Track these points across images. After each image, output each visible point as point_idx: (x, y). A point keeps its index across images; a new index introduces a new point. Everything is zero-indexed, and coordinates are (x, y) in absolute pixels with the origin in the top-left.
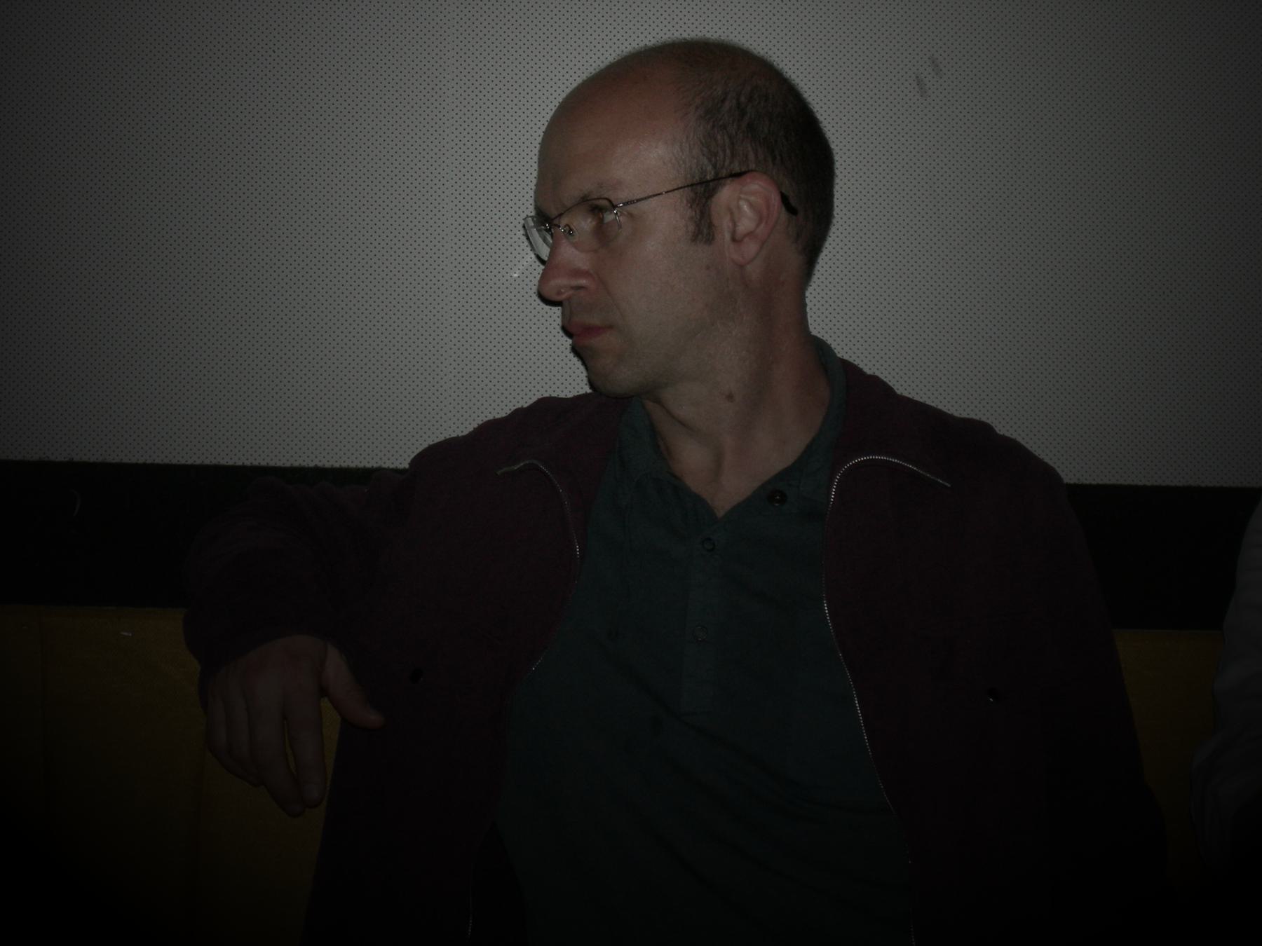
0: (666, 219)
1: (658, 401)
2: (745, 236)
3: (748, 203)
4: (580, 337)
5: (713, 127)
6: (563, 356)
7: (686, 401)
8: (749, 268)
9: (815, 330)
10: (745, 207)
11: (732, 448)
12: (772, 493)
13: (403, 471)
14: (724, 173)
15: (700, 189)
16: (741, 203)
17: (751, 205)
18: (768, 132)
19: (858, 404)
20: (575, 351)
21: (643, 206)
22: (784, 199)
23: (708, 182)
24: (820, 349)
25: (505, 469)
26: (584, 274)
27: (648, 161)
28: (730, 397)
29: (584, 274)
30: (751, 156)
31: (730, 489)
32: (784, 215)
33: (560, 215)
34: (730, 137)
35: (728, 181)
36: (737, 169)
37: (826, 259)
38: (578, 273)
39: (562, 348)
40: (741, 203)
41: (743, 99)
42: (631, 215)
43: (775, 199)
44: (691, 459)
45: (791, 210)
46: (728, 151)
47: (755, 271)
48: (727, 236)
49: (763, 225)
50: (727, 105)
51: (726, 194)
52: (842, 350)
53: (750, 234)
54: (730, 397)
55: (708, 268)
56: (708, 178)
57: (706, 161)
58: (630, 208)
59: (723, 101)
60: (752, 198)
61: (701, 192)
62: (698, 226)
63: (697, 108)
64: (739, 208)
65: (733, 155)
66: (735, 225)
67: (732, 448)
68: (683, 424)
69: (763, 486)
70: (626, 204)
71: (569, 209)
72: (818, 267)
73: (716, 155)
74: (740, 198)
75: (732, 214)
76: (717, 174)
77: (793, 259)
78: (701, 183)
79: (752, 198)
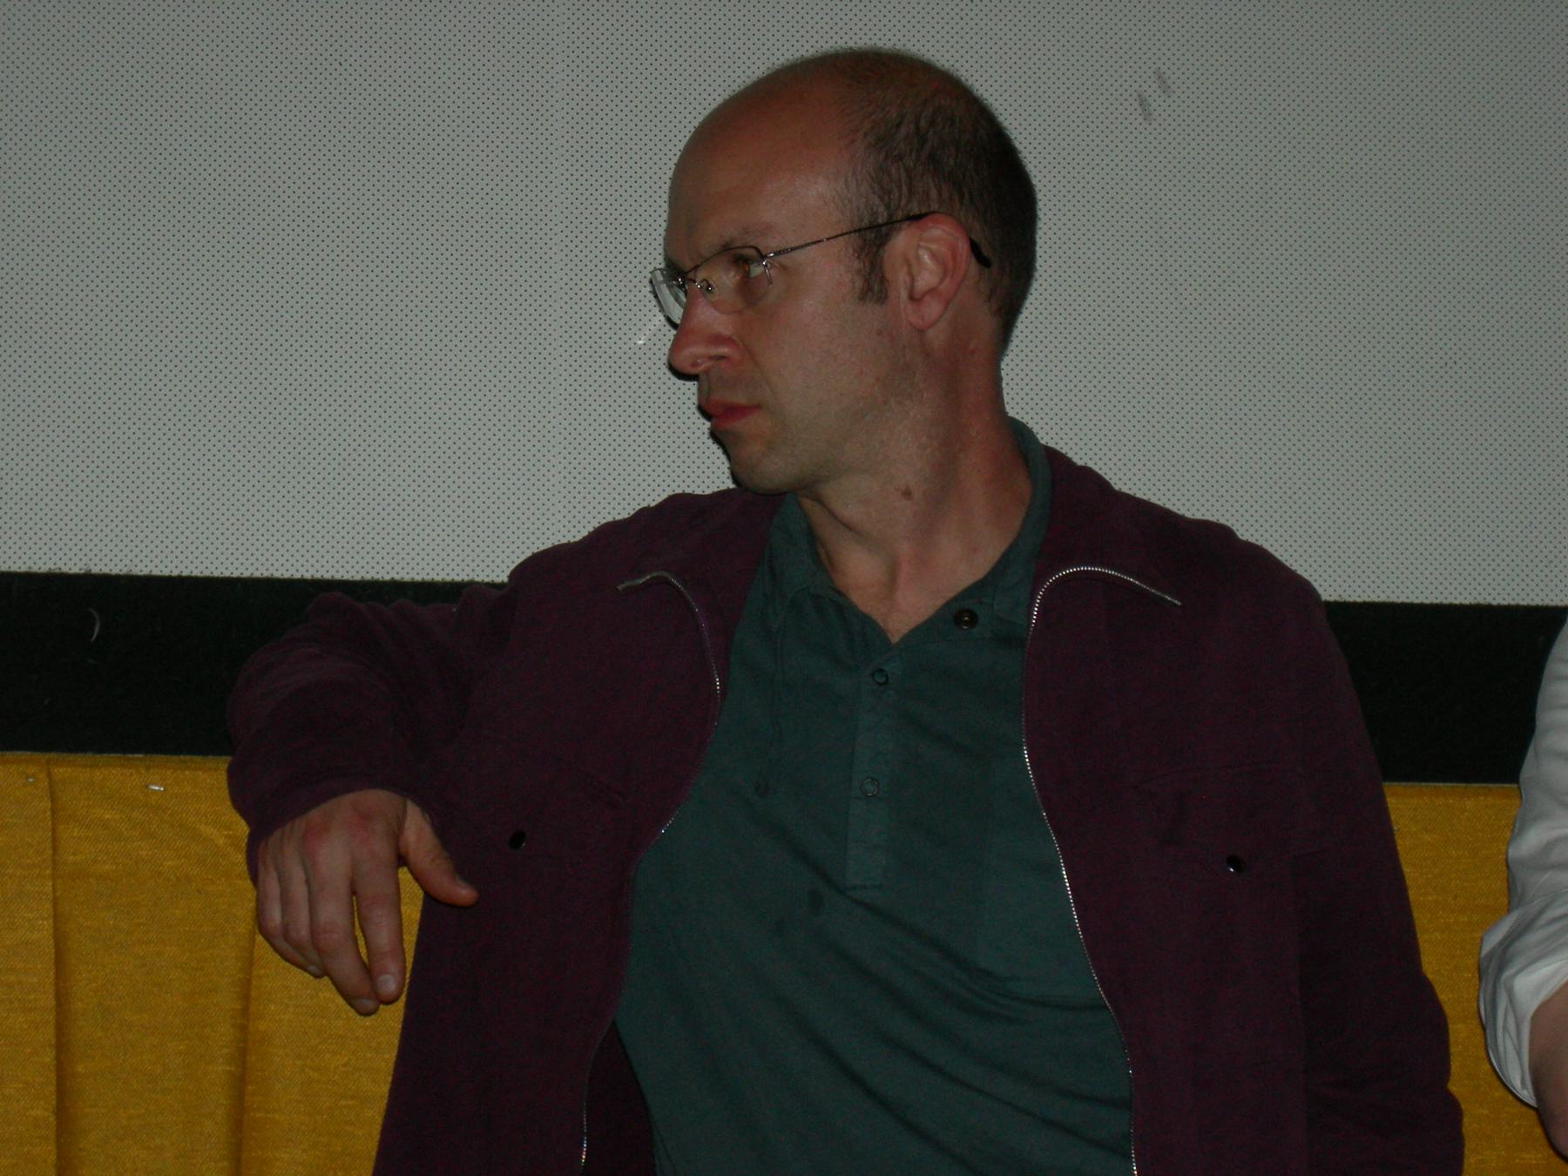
0: (827, 272)
1: (818, 499)
3: (929, 253)
4: (721, 419)
5: (886, 157)
7: (851, 498)
8: (931, 333)
10: (926, 258)
11: (910, 559)
12: (960, 613)
14: (900, 215)
16: (921, 252)
17: (933, 256)
18: (951, 168)
19: (1070, 506)
22: (975, 248)
25: (666, 574)
27: (806, 200)
30: (934, 194)
31: (906, 609)
32: (974, 267)
33: (696, 268)
34: (907, 170)
36: (915, 209)
38: (718, 340)
40: (921, 252)
41: (923, 123)
42: (784, 268)
43: (963, 248)
45: (983, 261)
46: (905, 189)
47: (937, 337)
48: (904, 294)
49: (947, 281)
50: (903, 131)
51: (902, 241)
53: (932, 291)
54: (907, 494)
55: (880, 333)
56: (880, 221)
57: (877, 201)
58: (783, 259)
59: (898, 126)
60: (934, 247)
61: (871, 239)
64: (918, 258)
65: (911, 192)
66: (913, 280)
67: (910, 559)
68: (848, 527)
69: (948, 603)
70: (778, 253)
72: (1016, 332)
73: (890, 193)
75: (909, 265)
76: (890, 216)
77: (985, 322)
78: (871, 228)
79: (934, 247)
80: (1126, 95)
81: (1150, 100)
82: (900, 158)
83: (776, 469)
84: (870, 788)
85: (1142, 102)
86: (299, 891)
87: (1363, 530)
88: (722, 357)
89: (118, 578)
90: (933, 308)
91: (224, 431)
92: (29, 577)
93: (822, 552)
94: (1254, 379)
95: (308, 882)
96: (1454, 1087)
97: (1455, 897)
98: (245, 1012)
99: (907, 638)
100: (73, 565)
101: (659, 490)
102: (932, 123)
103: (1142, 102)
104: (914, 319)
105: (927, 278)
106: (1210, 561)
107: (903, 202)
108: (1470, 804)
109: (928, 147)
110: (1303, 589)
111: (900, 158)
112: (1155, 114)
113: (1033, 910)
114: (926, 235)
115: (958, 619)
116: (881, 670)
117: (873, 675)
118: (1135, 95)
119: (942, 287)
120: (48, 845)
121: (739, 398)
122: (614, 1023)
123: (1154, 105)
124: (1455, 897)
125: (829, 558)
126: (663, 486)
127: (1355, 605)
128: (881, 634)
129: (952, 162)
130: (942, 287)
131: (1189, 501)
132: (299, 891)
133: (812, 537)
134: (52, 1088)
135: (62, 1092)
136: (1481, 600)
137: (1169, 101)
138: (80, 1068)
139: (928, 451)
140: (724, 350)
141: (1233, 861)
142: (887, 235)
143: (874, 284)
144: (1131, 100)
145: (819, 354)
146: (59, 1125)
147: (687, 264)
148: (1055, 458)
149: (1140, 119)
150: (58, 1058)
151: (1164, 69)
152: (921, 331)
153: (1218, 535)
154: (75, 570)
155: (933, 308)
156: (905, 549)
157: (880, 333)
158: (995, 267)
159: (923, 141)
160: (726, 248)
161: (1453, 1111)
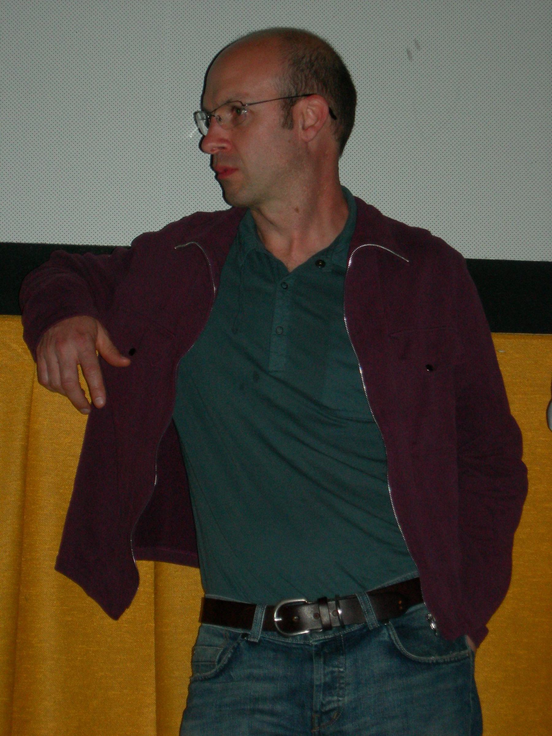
0: (269, 115)
1: (259, 211)
2: (309, 127)
3: (313, 110)
4: (221, 174)
5: (297, 70)
6: (210, 182)
7: (273, 210)
8: (310, 144)
9: (343, 182)
10: (311, 113)
11: (296, 237)
12: (318, 261)
13: (127, 247)
14: (301, 94)
15: (288, 101)
16: (309, 110)
17: (313, 112)
18: (323, 78)
19: (364, 220)
20: (216, 177)
21: (257, 107)
22: (331, 112)
23: (292, 97)
24: (345, 192)
25: (180, 246)
26: (226, 141)
27: (263, 86)
28: (297, 210)
29: (226, 141)
30: (315, 87)
31: (296, 259)
32: (329, 119)
33: (215, 110)
34: (305, 77)
35: (303, 98)
36: (308, 92)
37: (345, 160)
38: (222, 140)
39: (210, 178)
40: (309, 110)
41: (313, 58)
42: (251, 112)
43: (326, 110)
44: (277, 243)
45: (333, 117)
46: (304, 84)
47: (313, 146)
48: (300, 127)
49: (318, 123)
50: (304, 60)
51: (302, 105)
52: (355, 193)
53: (312, 127)
54: (297, 210)
55: (289, 141)
56: (293, 95)
57: (292, 87)
58: (251, 108)
59: (303, 58)
60: (314, 109)
61: (289, 102)
62: (286, 119)
63: (289, 60)
64: (307, 112)
65: (306, 85)
66: (304, 121)
67: (296, 237)
68: (271, 223)
69: (313, 257)
70: (250, 104)
71: (219, 107)
72: (346, 146)
73: (297, 84)
74: (308, 108)
75: (303, 115)
76: (297, 94)
77: (333, 144)
78: (288, 98)
79: (314, 109)
81: (412, 52)
82: (303, 70)
83: (244, 196)
84: (280, 331)
87: (480, 233)
88: (224, 148)
90: (312, 134)
93: (259, 234)
94: (442, 172)
96: (525, 459)
97: (528, 380)
98: (29, 420)
99: (296, 270)
101: (139, 231)
102: (317, 58)
103: (409, 52)
104: (304, 138)
105: (309, 122)
106: (421, 245)
107: (303, 88)
108: (535, 342)
109: (314, 68)
110: (456, 255)
111: (302, 70)
112: (414, 58)
113: (348, 384)
114: (310, 103)
115: (317, 263)
116: (284, 283)
117: (281, 285)
118: (405, 50)
119: (316, 125)
121: (230, 165)
124: (528, 380)
126: (141, 229)
127: (492, 261)
128: (285, 269)
129: (323, 75)
130: (316, 125)
131: (411, 220)
133: (256, 227)
136: (544, 260)
137: (419, 52)
139: (306, 193)
140: (224, 145)
141: (429, 367)
142: (295, 101)
143: (288, 121)
145: (264, 150)
147: (211, 108)
148: (358, 200)
151: (418, 39)
152: (306, 143)
153: (425, 233)
155: (312, 134)
156: (296, 234)
157: (289, 141)
158: (338, 120)
159: (313, 65)
160: (229, 102)
161: (524, 470)
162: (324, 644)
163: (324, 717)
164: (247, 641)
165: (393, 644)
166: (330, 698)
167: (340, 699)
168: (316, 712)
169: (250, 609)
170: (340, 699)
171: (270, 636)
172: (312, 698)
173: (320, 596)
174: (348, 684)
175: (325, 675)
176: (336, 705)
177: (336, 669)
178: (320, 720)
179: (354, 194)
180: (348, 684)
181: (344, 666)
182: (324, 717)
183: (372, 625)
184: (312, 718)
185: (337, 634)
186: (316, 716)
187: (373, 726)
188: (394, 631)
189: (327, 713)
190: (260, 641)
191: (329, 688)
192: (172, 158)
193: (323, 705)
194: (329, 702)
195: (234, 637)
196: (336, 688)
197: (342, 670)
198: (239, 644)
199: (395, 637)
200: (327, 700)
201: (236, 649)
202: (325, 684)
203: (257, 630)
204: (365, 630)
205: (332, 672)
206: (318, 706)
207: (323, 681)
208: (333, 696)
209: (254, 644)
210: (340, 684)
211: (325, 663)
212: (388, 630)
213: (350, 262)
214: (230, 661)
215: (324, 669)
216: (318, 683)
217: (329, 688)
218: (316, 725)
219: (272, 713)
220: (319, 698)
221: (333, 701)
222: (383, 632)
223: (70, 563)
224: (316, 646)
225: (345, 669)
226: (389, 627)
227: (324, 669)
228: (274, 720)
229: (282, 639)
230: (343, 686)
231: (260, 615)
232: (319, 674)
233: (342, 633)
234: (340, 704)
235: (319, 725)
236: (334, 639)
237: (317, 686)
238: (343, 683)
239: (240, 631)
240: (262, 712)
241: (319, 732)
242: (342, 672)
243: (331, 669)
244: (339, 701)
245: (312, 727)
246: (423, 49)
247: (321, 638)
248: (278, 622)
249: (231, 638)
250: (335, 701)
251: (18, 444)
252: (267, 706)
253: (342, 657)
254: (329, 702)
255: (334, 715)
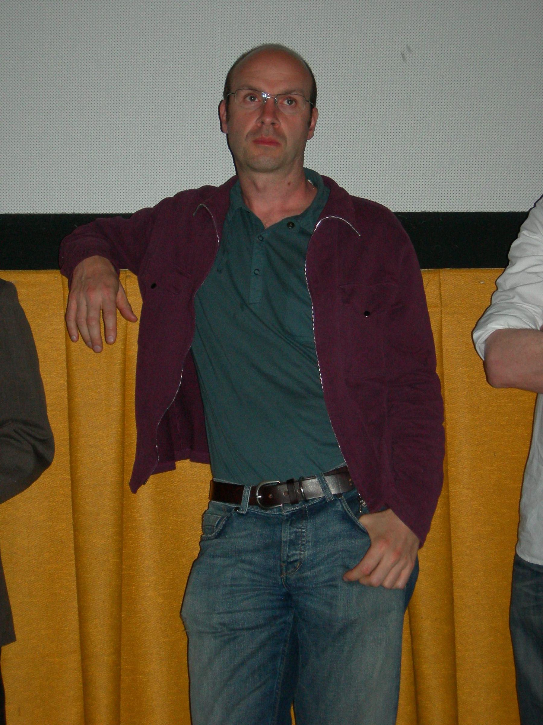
19: (328, 193)
67: (273, 203)
80: (397, 53)
85: (403, 55)
86: (84, 308)
89: (83, 215)
91: (342, 161)
92: (476, 213)
95: (87, 306)
98: (125, 349)
100: (69, 211)
103: (403, 55)
112: (407, 59)
115: (288, 225)
120: (62, 298)
122: (191, 350)
123: (406, 56)
125: (249, 203)
132: (84, 308)
134: (66, 374)
135: (69, 375)
136: (512, 211)
137: (405, 64)
138: (74, 368)
144: (399, 55)
146: (68, 386)
149: (402, 61)
150: (67, 365)
154: (70, 213)
161: (342, 189)
162: (293, 514)
163: (290, 566)
164: (238, 513)
165: (347, 514)
166: (294, 552)
167: (302, 553)
168: (284, 562)
169: (241, 488)
170: (302, 553)
171: (255, 509)
172: (280, 550)
173: (289, 478)
174: (307, 542)
175: (290, 534)
176: (298, 557)
177: (300, 530)
178: (287, 569)
179: (321, 174)
180: (307, 542)
181: (306, 528)
182: (290, 566)
183: (329, 498)
184: (281, 566)
185: (303, 506)
186: (284, 565)
187: (326, 573)
188: (346, 504)
189: (291, 563)
190: (247, 513)
191: (293, 543)
192: (366, 181)
193: (288, 557)
194: (293, 555)
195: (229, 510)
196: (299, 544)
197: (304, 531)
198: (231, 514)
199: (347, 508)
200: (292, 553)
201: (228, 518)
202: (290, 540)
203: (245, 506)
204: (324, 502)
205: (296, 532)
206: (285, 558)
207: (288, 538)
208: (296, 550)
209: (242, 514)
210: (302, 541)
211: (290, 525)
212: (341, 503)
213: (318, 224)
214: (225, 526)
215: (290, 529)
216: (285, 540)
217: (293, 543)
218: (284, 572)
219: (250, 563)
220: (286, 551)
221: (296, 554)
222: (337, 504)
223: (131, 484)
224: (287, 516)
225: (307, 530)
226: (342, 501)
227: (290, 529)
228: (252, 568)
229: (264, 511)
230: (304, 543)
231: (247, 494)
232: (286, 534)
233: (306, 505)
234: (302, 556)
235: (286, 572)
236: (301, 510)
237: (284, 542)
238: (304, 541)
239: (233, 506)
240: (243, 561)
241: (286, 577)
242: (304, 532)
243: (295, 529)
244: (301, 554)
245: (281, 573)
246: (408, 61)
247: (291, 510)
248: (259, 498)
249: (227, 511)
250: (297, 554)
251: (118, 367)
252: (248, 557)
253: (305, 521)
254: (293, 555)
255: (297, 565)
